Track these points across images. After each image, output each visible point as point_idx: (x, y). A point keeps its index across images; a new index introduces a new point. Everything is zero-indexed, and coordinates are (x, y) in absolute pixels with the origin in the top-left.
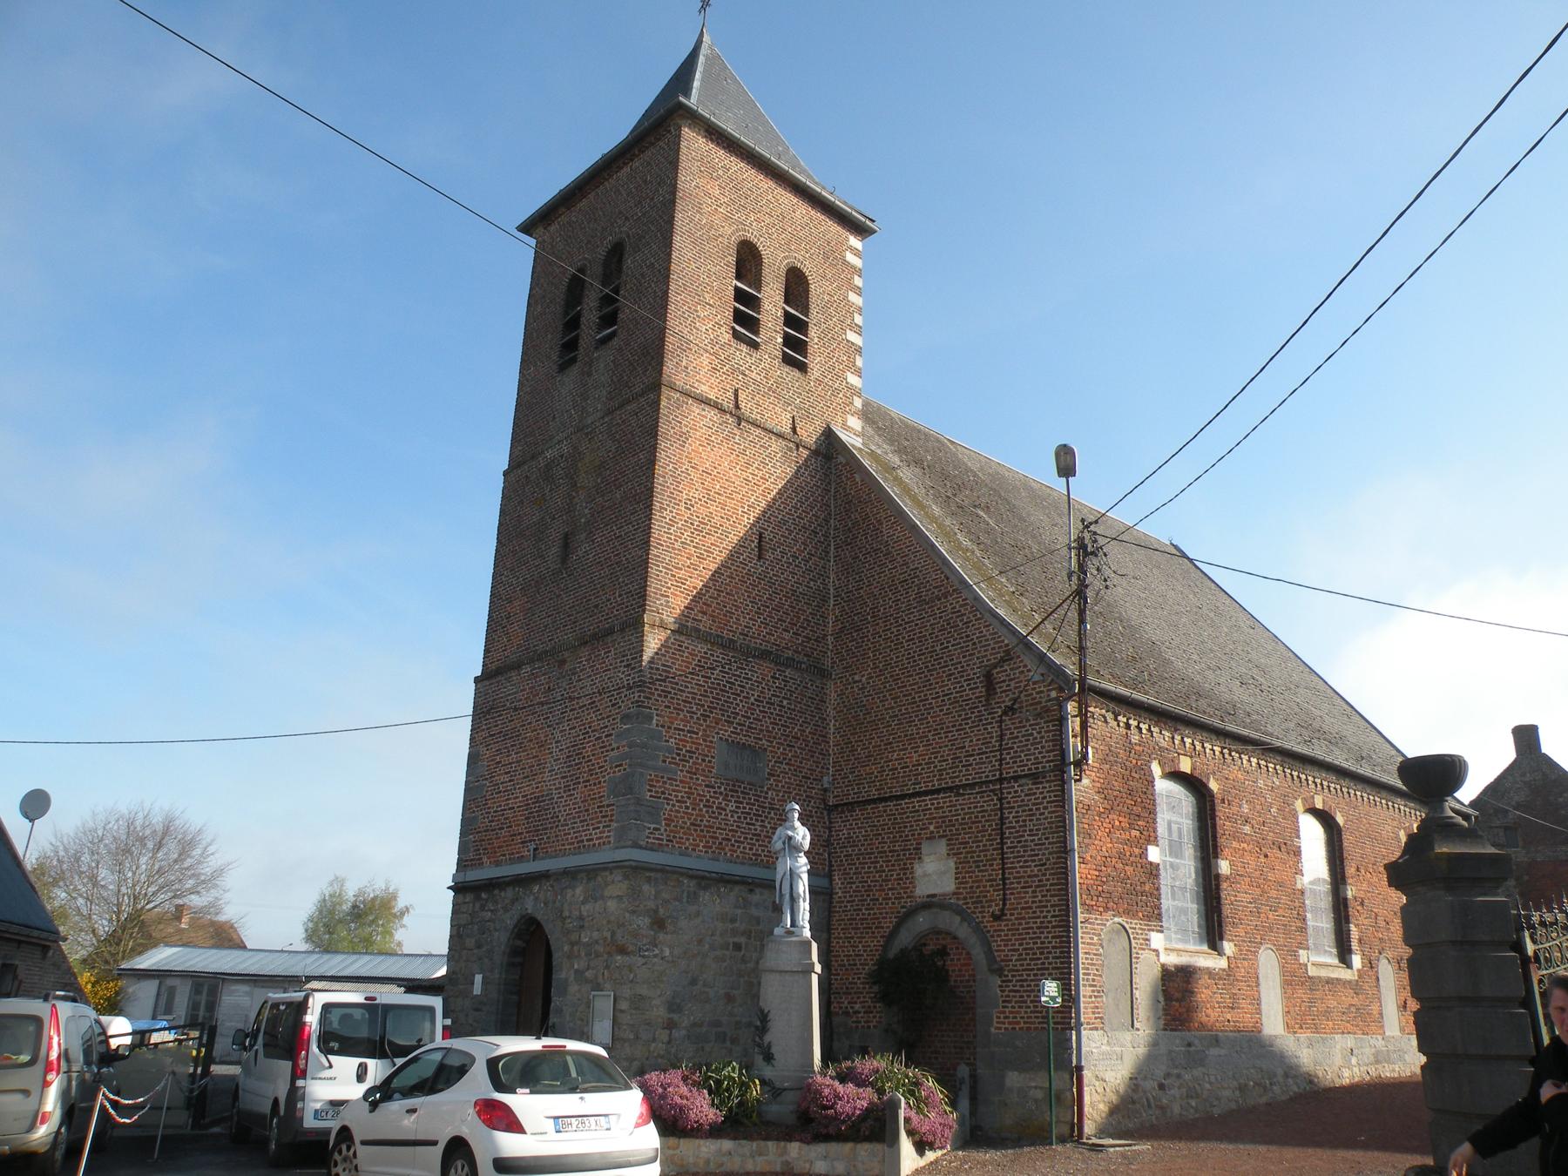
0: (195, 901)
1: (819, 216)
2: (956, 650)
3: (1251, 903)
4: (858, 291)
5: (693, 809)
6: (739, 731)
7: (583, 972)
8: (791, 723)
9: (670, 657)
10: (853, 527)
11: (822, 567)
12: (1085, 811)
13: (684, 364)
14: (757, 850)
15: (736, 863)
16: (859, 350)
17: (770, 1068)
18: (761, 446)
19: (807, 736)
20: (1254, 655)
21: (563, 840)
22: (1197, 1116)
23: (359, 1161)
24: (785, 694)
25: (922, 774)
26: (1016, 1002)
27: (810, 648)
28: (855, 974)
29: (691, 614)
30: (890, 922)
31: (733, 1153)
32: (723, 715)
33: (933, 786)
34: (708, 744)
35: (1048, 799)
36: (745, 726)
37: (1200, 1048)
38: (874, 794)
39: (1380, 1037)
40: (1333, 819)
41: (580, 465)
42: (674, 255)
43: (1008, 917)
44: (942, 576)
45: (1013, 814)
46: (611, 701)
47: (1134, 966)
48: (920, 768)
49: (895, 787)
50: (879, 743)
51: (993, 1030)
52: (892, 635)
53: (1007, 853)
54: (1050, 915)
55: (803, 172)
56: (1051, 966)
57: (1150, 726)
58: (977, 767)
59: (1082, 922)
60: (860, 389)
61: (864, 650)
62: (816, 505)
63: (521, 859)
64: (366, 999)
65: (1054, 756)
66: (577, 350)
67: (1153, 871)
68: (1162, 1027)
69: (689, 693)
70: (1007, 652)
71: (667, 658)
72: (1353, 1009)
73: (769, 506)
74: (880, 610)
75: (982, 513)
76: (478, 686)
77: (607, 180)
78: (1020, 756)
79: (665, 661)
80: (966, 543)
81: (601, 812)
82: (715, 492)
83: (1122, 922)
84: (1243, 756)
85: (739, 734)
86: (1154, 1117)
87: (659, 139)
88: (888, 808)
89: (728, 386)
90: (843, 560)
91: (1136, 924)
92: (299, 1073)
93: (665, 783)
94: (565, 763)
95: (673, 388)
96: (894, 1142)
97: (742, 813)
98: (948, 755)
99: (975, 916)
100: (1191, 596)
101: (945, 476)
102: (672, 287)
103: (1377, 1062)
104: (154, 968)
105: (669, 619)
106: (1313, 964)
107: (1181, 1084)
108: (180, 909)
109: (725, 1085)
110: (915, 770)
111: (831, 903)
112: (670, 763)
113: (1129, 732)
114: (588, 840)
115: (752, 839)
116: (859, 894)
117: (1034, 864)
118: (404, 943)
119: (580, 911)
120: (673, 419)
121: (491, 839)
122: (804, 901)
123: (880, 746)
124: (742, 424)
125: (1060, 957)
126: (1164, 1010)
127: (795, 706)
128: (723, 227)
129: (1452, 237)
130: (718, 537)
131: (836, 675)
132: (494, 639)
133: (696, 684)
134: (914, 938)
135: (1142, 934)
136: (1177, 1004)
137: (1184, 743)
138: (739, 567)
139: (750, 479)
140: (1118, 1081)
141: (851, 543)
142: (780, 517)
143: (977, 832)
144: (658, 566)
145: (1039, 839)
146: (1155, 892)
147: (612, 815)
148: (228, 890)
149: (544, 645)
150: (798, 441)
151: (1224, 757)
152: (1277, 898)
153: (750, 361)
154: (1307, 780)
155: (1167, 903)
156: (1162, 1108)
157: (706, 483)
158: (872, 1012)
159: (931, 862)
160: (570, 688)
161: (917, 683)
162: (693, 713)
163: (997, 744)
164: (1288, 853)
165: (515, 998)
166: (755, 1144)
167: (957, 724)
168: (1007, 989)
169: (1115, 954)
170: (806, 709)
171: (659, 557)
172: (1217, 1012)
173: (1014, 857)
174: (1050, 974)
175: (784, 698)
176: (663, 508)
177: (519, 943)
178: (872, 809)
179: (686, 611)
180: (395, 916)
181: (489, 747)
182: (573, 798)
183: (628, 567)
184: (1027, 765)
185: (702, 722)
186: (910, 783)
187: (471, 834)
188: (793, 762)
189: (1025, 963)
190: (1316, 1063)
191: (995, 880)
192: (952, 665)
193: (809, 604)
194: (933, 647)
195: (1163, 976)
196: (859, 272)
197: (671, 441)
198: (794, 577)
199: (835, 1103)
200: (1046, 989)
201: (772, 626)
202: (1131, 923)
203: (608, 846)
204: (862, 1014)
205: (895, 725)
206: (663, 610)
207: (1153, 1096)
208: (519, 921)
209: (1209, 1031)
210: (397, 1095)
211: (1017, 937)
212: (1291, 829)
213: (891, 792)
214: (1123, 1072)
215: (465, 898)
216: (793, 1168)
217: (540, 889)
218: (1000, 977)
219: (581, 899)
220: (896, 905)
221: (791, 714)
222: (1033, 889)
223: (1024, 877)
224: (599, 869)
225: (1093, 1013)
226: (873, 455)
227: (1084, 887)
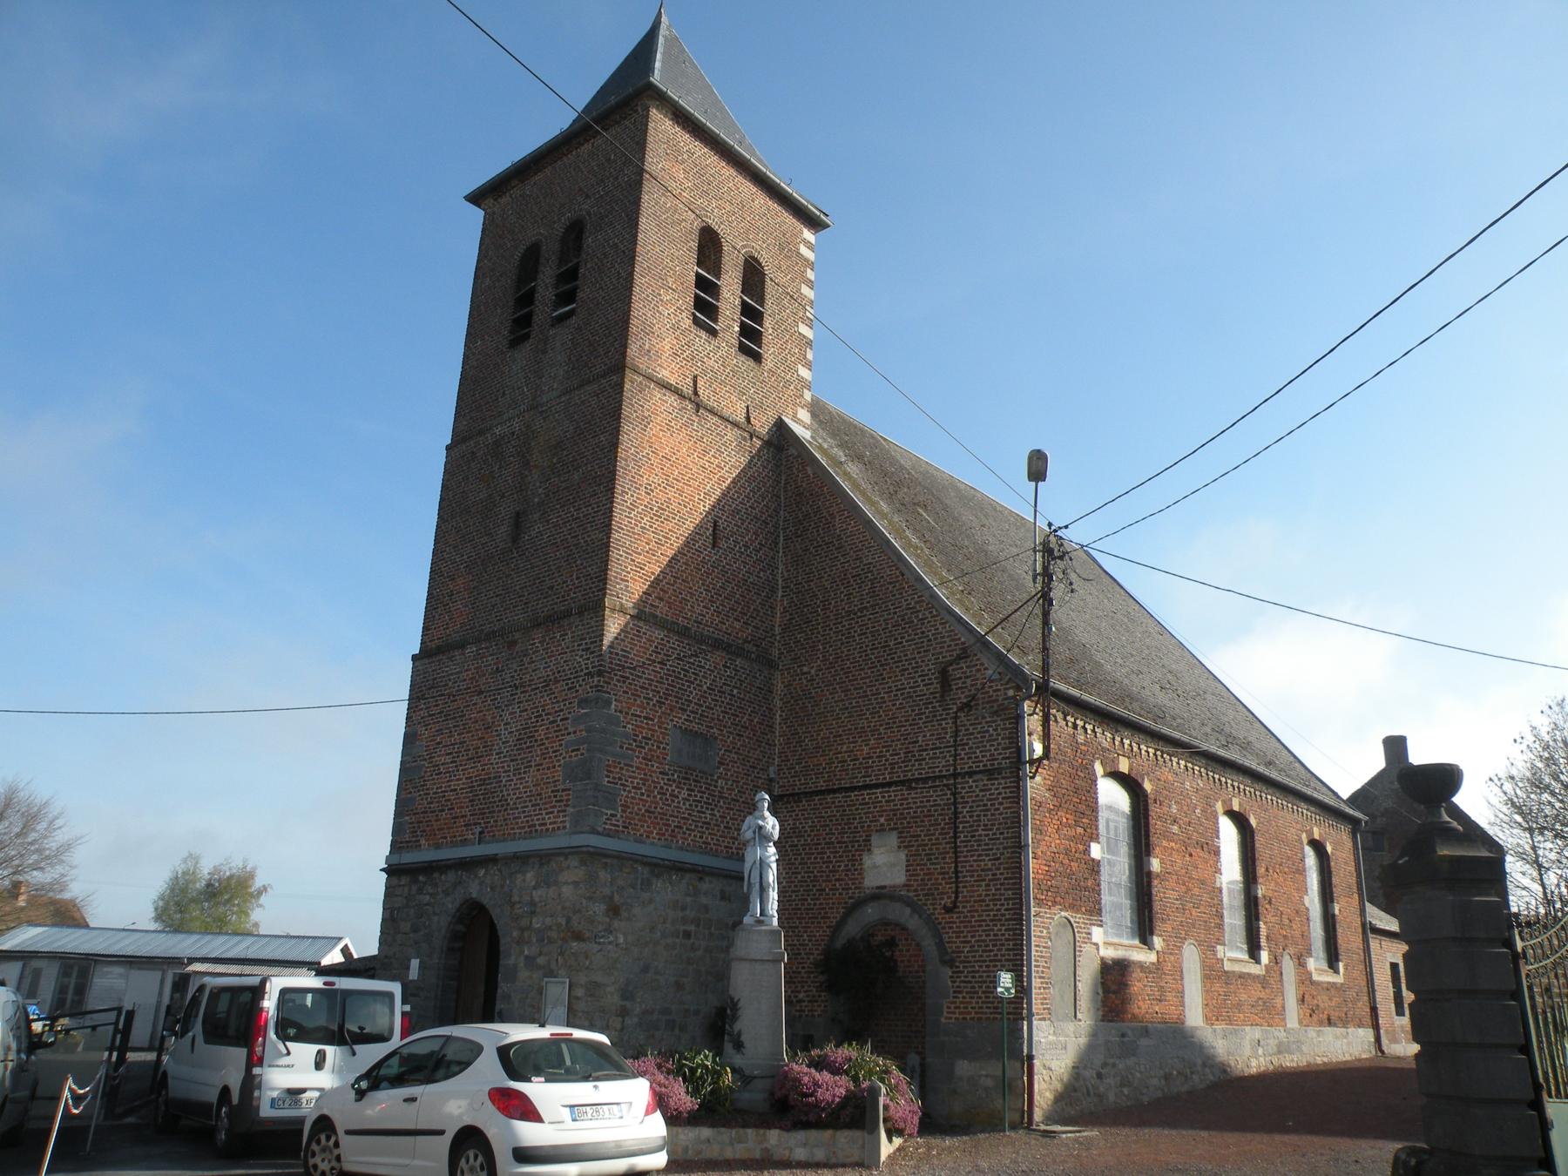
0: (37, 877)
1: (775, 206)
2: (910, 645)
3: (1177, 900)
4: (810, 284)
5: (648, 796)
6: (691, 718)
7: (534, 958)
10: (804, 520)
11: (772, 558)
13: (647, 347)
14: (707, 838)
15: (687, 851)
16: (809, 343)
18: (717, 434)
21: (512, 824)
23: (342, 1150)
24: (736, 683)
25: (873, 767)
26: (967, 993)
30: (838, 913)
31: (711, 1141)
33: (885, 778)
35: (1004, 795)
38: (822, 785)
39: (1282, 1029)
40: (1247, 821)
41: (533, 444)
42: (640, 236)
44: (898, 572)
45: (967, 809)
46: (567, 684)
47: (1077, 959)
48: (870, 761)
49: (844, 779)
50: (828, 735)
51: (943, 1020)
52: (844, 629)
53: (960, 847)
56: (1003, 958)
57: (1094, 726)
60: (810, 382)
61: (814, 642)
63: (465, 842)
64: (325, 984)
65: (1010, 753)
67: (1094, 867)
68: (1100, 1018)
69: (645, 678)
70: (964, 650)
72: (1260, 1003)
74: (830, 604)
75: (920, 510)
76: (416, 665)
80: (915, 540)
81: (555, 796)
82: (673, 479)
84: (1173, 758)
85: (691, 721)
86: (1092, 1104)
87: (625, 118)
89: (688, 372)
90: (793, 552)
91: (1080, 918)
92: (254, 1060)
93: (622, 769)
94: (515, 745)
97: (694, 801)
98: (901, 749)
99: (926, 908)
100: (1106, 601)
103: (1280, 1052)
104: (18, 949)
106: (1228, 960)
109: (698, 1074)
112: (626, 748)
114: (540, 825)
115: (702, 827)
116: (804, 884)
117: (988, 858)
118: (261, 924)
119: (532, 897)
120: (636, 402)
121: (430, 821)
123: (829, 738)
125: (1013, 949)
126: (1103, 1002)
127: (745, 695)
129: (1507, 284)
130: (675, 524)
131: (783, 666)
132: (434, 616)
136: (1114, 996)
138: (694, 554)
139: (707, 467)
140: (1063, 1070)
141: (802, 535)
142: (734, 505)
143: (930, 826)
144: (619, 550)
145: (994, 834)
146: (1097, 888)
147: (568, 800)
148: (76, 867)
149: (492, 625)
150: (752, 431)
152: (1198, 896)
154: (1226, 783)
155: (1106, 899)
156: (1099, 1096)
157: (665, 469)
158: (816, 1001)
159: (882, 853)
160: (521, 670)
161: (869, 677)
162: (649, 699)
164: (1209, 853)
166: (734, 1132)
168: (958, 980)
169: (1062, 947)
171: (620, 541)
173: (968, 851)
175: (734, 687)
176: (625, 492)
177: (461, 928)
178: (819, 800)
179: (644, 596)
180: (252, 895)
181: (429, 727)
182: (523, 781)
183: (587, 549)
185: (657, 708)
186: (860, 775)
187: (408, 815)
188: (741, 752)
190: (1229, 1054)
191: (948, 873)
192: (906, 660)
193: (759, 594)
194: (886, 642)
195: (1102, 968)
196: (812, 266)
198: (745, 567)
199: (815, 1091)
200: (1002, 980)
203: (563, 831)
204: (806, 1003)
205: (845, 718)
206: (622, 594)
207: (1092, 1085)
208: (461, 905)
209: (1140, 1022)
210: (384, 1084)
212: (1212, 829)
213: (839, 784)
214: (1067, 1061)
217: (485, 874)
218: (951, 968)
219: (533, 883)
220: (844, 895)
221: (740, 703)
224: (553, 855)
225: (1042, 1004)
226: (820, 448)
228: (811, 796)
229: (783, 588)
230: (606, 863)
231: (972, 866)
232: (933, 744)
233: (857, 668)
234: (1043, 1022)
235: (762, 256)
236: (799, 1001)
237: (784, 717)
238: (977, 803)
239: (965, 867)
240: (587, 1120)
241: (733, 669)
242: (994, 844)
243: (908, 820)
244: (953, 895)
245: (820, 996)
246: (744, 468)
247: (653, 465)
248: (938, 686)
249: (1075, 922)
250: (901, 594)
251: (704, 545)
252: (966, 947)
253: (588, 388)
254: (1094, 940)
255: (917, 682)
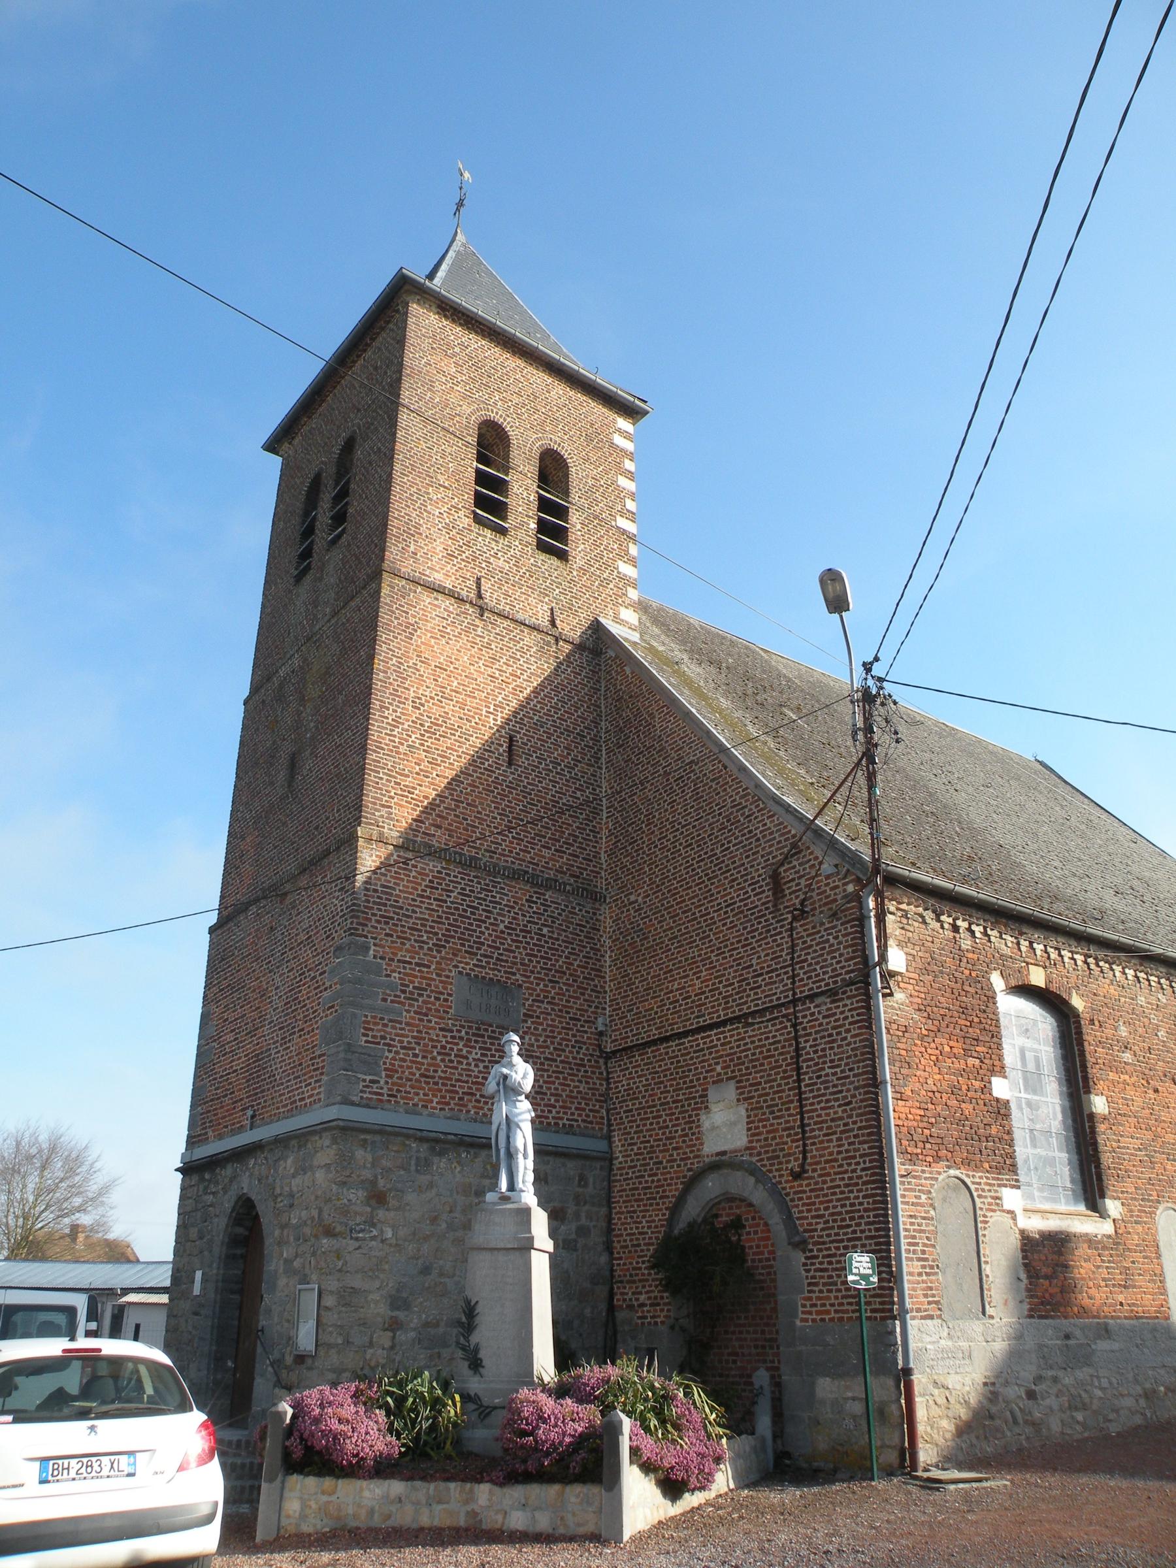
0: (85, 1219)
3: (1140, 1150)
5: (424, 1057)
7: (292, 1262)
8: (553, 955)
9: (391, 877)
10: (625, 727)
11: (592, 775)
12: (900, 1034)
13: (412, 548)
16: (632, 538)
17: (477, 1378)
18: (510, 639)
19: (576, 970)
20: (1135, 868)
22: (1086, 1435)
24: (545, 920)
26: (824, 1284)
27: (578, 867)
28: (639, 1257)
29: (421, 827)
30: (676, 1190)
32: (463, 945)
34: (443, 979)
35: (850, 1020)
36: (492, 958)
37: (1083, 1341)
38: (655, 1033)
42: (399, 434)
43: (810, 1174)
47: (980, 1233)
48: (703, 997)
49: (676, 1023)
51: (798, 1323)
53: (805, 1092)
54: (859, 1167)
55: (566, 357)
57: (985, 928)
58: (766, 988)
59: (902, 1176)
60: (635, 580)
61: (640, 865)
62: (583, 706)
63: (241, 1129)
65: (855, 964)
66: (311, 557)
67: (1001, 1110)
69: (416, 918)
71: (388, 878)
73: (522, 707)
74: (654, 817)
77: (343, 377)
78: (815, 970)
79: (385, 881)
83: (960, 1175)
84: (1114, 967)
85: (482, 967)
86: (1023, 1437)
88: (670, 1050)
91: (981, 1178)
93: (385, 1025)
95: (396, 574)
96: (610, 1480)
98: (734, 977)
99: (771, 1175)
100: (1057, 809)
101: (747, 677)
102: (397, 467)
105: (393, 833)
107: (1060, 1390)
108: (75, 1229)
110: (698, 1000)
111: (611, 1170)
113: (957, 936)
116: (641, 1157)
120: (397, 608)
122: (525, 1157)
123: (659, 975)
124: (486, 615)
126: (1028, 1290)
127: (558, 934)
128: (461, 406)
131: (611, 898)
133: (426, 908)
134: (703, 1208)
135: (990, 1191)
137: (1034, 949)
138: (483, 774)
139: (497, 675)
140: (968, 1388)
142: (536, 718)
145: (842, 1072)
151: (1089, 968)
153: (496, 548)
155: (1023, 1150)
157: (440, 680)
161: (697, 896)
162: (423, 942)
163: (789, 957)
165: (236, 1297)
166: (432, 1486)
167: (743, 938)
168: (813, 1268)
170: (573, 938)
171: (379, 762)
172: (1104, 1293)
173: (814, 1097)
174: (863, 1246)
176: (385, 707)
177: (240, 1230)
178: (652, 1052)
179: (415, 824)
184: (824, 980)
185: (435, 953)
186: (693, 1016)
187: (200, 1105)
189: (832, 1232)
194: (712, 850)
195: (1023, 1245)
197: (394, 632)
199: (537, 1427)
200: (855, 1264)
201: (527, 842)
202: (973, 1176)
205: (675, 948)
207: (1020, 1408)
208: (236, 1203)
209: (1094, 1317)
211: (821, 1199)
213: (672, 1029)
215: (191, 1180)
216: (481, 1521)
217: (255, 1164)
218: (804, 1253)
219: (292, 1171)
222: (838, 1135)
223: (826, 1121)
225: (926, 1296)
226: (651, 650)
227: (904, 1130)
228: (644, 1049)
229: (607, 808)
230: (365, 1141)
231: (819, 1116)
232: (768, 966)
233: (685, 887)
234: (929, 1322)
235: (563, 447)
236: (643, 1305)
237: (614, 958)
238: (822, 1034)
239: (812, 1118)
240: (67, 1480)
241: (541, 904)
242: (843, 1085)
243: (746, 1065)
244: (801, 1156)
245: (662, 1298)
246: (549, 676)
247: (423, 676)
248: (770, 893)
249: (973, 1183)
250: (725, 790)
251: (496, 763)
252: (820, 1223)
253: (353, 604)
254: (1006, 1207)
255: (747, 892)
